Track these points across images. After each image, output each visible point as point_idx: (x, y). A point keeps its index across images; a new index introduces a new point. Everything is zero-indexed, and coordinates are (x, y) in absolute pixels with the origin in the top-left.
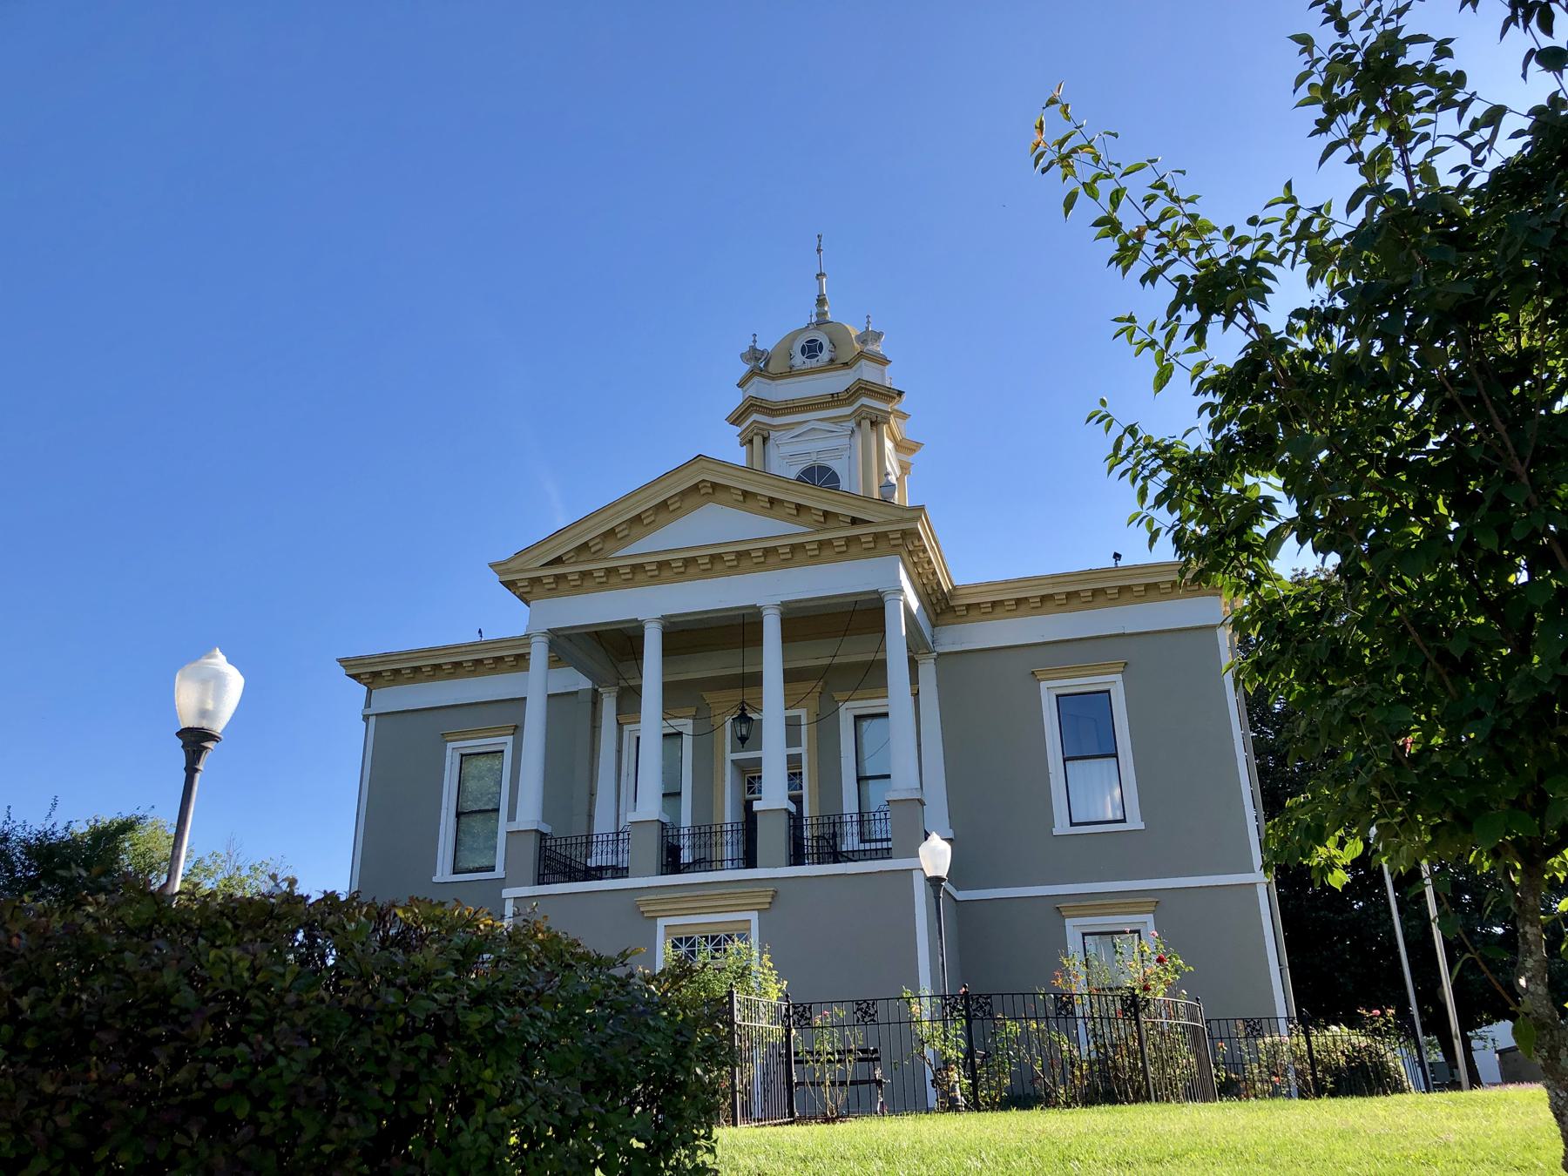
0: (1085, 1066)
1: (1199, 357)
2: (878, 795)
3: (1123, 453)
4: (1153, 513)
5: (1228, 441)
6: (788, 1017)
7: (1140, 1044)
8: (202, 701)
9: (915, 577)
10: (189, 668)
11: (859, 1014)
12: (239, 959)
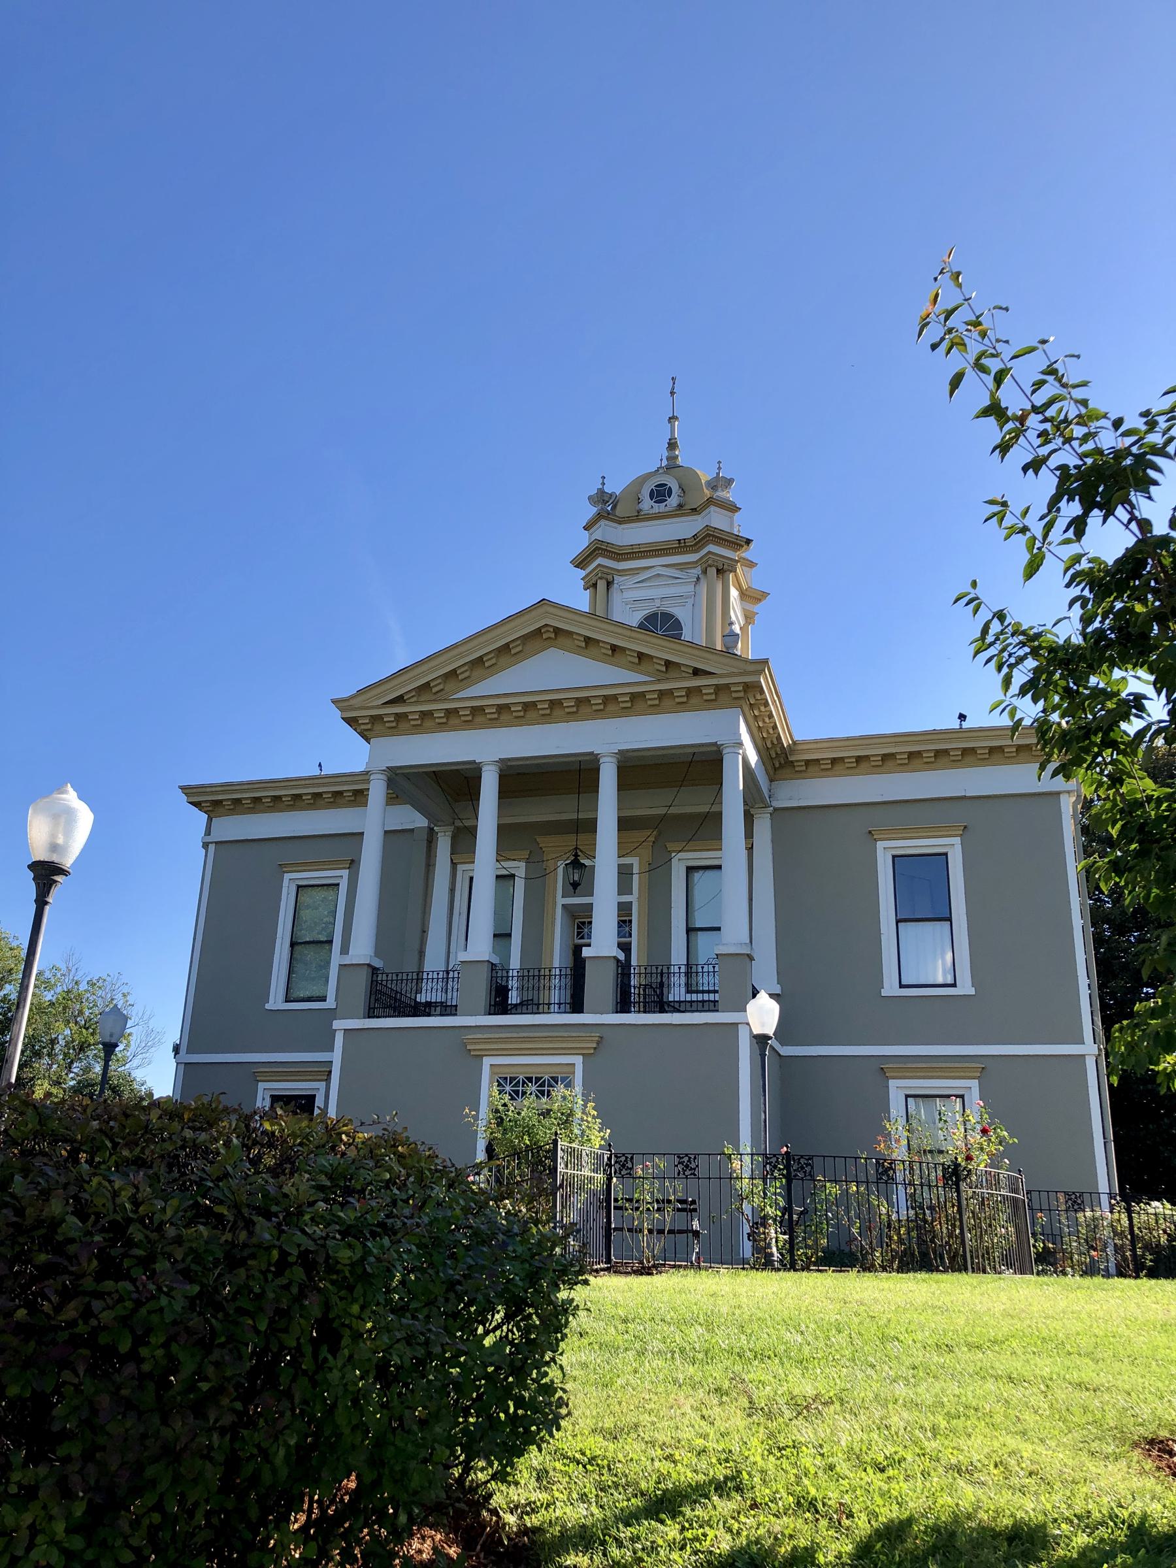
0: (903, 1231)
1: (1074, 549)
2: (707, 948)
3: (990, 639)
4: (1017, 702)
5: (1100, 634)
6: (610, 1166)
7: (960, 1211)
8: (53, 835)
9: (755, 730)
10: (42, 803)
11: (680, 1167)
12: (121, 1189)
